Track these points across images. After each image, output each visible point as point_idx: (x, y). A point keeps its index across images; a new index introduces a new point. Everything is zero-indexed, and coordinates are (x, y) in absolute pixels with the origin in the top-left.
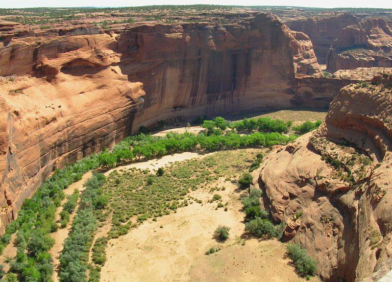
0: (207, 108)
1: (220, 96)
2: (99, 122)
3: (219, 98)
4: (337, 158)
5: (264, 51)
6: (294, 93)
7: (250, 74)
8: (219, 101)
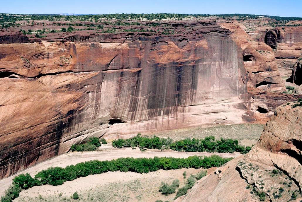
0: (148, 124)
1: (162, 112)
2: (19, 138)
3: (162, 114)
4: (262, 188)
5: (213, 63)
6: (246, 108)
7: (196, 89)
8: (161, 117)
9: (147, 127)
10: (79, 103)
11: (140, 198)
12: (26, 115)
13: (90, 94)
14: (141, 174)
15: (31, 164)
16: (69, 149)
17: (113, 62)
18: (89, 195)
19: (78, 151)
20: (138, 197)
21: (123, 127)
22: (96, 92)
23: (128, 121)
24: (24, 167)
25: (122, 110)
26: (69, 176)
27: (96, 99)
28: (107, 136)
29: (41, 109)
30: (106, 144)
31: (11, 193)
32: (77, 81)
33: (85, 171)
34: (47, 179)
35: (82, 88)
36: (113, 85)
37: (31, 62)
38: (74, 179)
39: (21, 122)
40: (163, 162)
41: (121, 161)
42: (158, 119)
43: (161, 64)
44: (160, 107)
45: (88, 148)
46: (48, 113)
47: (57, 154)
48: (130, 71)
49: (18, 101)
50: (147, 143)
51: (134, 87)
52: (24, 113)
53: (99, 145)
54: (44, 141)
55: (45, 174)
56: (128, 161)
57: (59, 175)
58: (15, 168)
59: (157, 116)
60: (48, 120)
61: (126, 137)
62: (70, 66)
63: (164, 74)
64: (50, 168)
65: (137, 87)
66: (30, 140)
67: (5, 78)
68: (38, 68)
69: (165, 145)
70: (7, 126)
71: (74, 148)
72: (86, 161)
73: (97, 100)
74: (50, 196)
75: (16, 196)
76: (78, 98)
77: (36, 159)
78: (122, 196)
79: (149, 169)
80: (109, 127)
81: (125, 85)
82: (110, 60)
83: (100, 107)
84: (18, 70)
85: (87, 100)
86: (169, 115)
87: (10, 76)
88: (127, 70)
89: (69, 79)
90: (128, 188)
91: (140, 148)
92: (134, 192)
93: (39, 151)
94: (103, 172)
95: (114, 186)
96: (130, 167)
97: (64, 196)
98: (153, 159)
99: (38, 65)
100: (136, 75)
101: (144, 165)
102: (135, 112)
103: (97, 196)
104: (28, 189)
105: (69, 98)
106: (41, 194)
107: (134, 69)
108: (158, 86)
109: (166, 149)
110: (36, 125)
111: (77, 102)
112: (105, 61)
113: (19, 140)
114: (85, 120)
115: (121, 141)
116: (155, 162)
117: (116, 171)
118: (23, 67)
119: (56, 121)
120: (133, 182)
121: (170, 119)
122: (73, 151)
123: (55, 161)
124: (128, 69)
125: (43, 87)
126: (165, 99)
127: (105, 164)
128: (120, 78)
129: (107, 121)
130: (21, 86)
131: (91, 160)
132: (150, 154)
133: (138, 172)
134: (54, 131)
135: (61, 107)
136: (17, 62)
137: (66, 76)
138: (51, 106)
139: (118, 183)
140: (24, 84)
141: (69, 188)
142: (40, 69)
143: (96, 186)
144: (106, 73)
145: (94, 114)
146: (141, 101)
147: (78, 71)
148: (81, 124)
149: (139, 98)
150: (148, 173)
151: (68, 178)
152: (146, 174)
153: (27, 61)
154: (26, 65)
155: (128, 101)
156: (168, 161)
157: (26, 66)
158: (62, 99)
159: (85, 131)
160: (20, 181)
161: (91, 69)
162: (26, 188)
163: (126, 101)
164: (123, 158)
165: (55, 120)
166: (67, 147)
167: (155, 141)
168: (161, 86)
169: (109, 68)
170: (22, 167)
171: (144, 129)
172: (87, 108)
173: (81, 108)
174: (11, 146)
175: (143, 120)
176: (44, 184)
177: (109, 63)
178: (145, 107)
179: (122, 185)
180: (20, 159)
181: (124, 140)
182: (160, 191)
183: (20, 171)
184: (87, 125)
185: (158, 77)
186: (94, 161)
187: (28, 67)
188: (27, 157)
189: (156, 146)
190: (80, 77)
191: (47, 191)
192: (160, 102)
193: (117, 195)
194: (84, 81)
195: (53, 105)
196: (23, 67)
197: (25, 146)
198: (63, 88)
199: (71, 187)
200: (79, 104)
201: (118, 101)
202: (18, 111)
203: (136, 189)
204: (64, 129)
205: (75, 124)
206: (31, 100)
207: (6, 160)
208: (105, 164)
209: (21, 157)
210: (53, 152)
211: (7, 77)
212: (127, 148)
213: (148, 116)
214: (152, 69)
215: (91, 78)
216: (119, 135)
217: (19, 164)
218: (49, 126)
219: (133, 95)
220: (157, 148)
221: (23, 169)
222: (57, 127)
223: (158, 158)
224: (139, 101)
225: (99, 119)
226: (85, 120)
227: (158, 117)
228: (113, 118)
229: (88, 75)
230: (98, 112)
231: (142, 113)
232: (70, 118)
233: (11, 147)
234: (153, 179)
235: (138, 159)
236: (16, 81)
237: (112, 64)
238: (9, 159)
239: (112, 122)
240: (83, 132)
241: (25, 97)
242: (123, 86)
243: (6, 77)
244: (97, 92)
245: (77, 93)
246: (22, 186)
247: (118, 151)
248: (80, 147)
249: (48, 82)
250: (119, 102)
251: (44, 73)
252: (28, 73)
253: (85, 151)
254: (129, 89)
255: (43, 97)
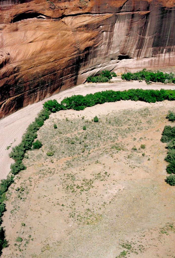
0: (152, 60)
1: (165, 50)
2: (46, 70)
8: (163, 55)
9: (151, 63)
10: (95, 41)
11: (150, 123)
12: (51, 50)
13: (104, 33)
14: (149, 103)
15: (55, 92)
16: (86, 80)
17: (125, 5)
18: (107, 119)
19: (93, 82)
20: (149, 122)
21: (130, 63)
22: (109, 32)
23: (134, 58)
24: (50, 94)
25: (130, 48)
26: (89, 103)
27: (109, 38)
28: (116, 70)
29: (63, 46)
30: (116, 77)
31: (43, 115)
32: (94, 22)
33: (102, 99)
34: (71, 105)
35: (98, 28)
36: (124, 26)
37: (55, 5)
38: (93, 106)
39: (46, 56)
40: (168, 94)
41: (132, 92)
42: (161, 56)
43: (167, 7)
44: (164, 46)
45: (101, 80)
46: (69, 49)
47: (75, 84)
48: (139, 13)
49: (44, 38)
50: (153, 77)
51: (142, 27)
52: (50, 49)
53: (110, 77)
54: (66, 73)
55: (69, 100)
56: (138, 92)
57: (81, 101)
58: (43, 95)
59: (159, 54)
60: (69, 55)
61: (133, 71)
62: (88, 8)
63: (169, 17)
64: (73, 95)
65: (144, 28)
66: (54, 72)
67: (33, 19)
68: (62, 10)
69: (168, 79)
70: (36, 59)
71: (89, 80)
72: (102, 91)
73: (110, 39)
74: (75, 119)
75: (47, 118)
76: (94, 36)
77: (59, 88)
78: (134, 121)
79: (156, 99)
80: (118, 62)
81: (135, 26)
82: (122, 3)
83: (112, 44)
84: (45, 11)
85: (101, 38)
86: (170, 53)
87: (38, 17)
88: (137, 12)
89: (87, 20)
90: (139, 114)
91: (146, 81)
92: (145, 118)
93: (62, 81)
94: (117, 100)
95: (127, 112)
96: (140, 97)
97: (86, 119)
98: (159, 90)
99: (61, 7)
100: (145, 17)
101: (152, 96)
102: (141, 50)
103: (114, 120)
104: (55, 112)
105: (87, 37)
106: (67, 117)
107: (144, 11)
108: (163, 28)
109: (168, 82)
110: (59, 59)
111: (93, 40)
112: (119, 4)
113: (46, 72)
114: (99, 56)
115: (130, 75)
116: (161, 93)
117: (127, 100)
118: (49, 9)
119: (75, 56)
120: (143, 109)
121: (171, 56)
122: (89, 82)
123: (74, 90)
124: (138, 12)
125: (65, 27)
126: (168, 39)
127: (119, 94)
128: (130, 20)
129: (117, 57)
130: (47, 25)
131: (106, 90)
132: (156, 87)
133: (146, 102)
134: (74, 64)
135: (80, 44)
136: (44, 5)
137: (84, 17)
138: (72, 43)
139: (158, 108)
140: (50, 24)
141: (90, 113)
142: (63, 11)
143: (112, 112)
144: (119, 15)
145: (107, 50)
146: (148, 40)
147: (94, 13)
148: (95, 59)
149: (146, 37)
150: (155, 102)
151: (88, 104)
152: (153, 103)
153: (52, 4)
154: (51, 7)
155: (136, 40)
156: (173, 93)
157: (51, 8)
158: (81, 38)
159: (99, 65)
160: (49, 105)
161: (106, 11)
162: (54, 112)
163: (135, 40)
164: (134, 89)
165: (75, 55)
166: (84, 78)
167: (159, 75)
168: (166, 28)
169: (122, 10)
170: (48, 95)
171: (148, 65)
172: (101, 46)
173: (96, 46)
174: (39, 76)
175: (147, 57)
176: (69, 109)
177: (121, 6)
178: (151, 45)
179: (134, 111)
180: (47, 88)
181: (132, 73)
182: (167, 118)
183: (47, 98)
184: (100, 60)
185: (164, 19)
186: (109, 91)
187: (53, 9)
188: (52, 86)
189: (160, 80)
190: (97, 18)
191: (72, 114)
192: (164, 41)
193: (131, 120)
194: (100, 21)
195: (73, 42)
196: (49, 9)
197: (51, 77)
198: (81, 27)
199: (91, 112)
200: (95, 42)
201: (128, 39)
202: (44, 47)
203: (146, 116)
204: (82, 63)
205: (91, 58)
206: (56, 37)
207: (36, 88)
208: (119, 94)
209: (48, 86)
210: (72, 82)
211: (36, 18)
212: (134, 81)
213: (152, 53)
214: (159, 12)
215: (106, 19)
216: (127, 69)
217: (46, 92)
218: (69, 60)
219: (141, 35)
220: (160, 82)
221: (50, 95)
222: (76, 61)
223: (164, 90)
224: (146, 40)
225: (110, 55)
226: (99, 56)
227: (160, 54)
228: (121, 54)
229: (104, 17)
230: (110, 48)
231: (147, 50)
232: (87, 53)
233: (40, 77)
234: (160, 108)
235: (146, 90)
236: (43, 21)
237: (125, 7)
238: (39, 87)
239: (121, 58)
240: (96, 66)
241: (50, 35)
242: (133, 26)
243: (34, 18)
244: (110, 32)
245: (93, 32)
246: (50, 109)
247: (127, 83)
248: (95, 78)
249: (70, 22)
250: (128, 41)
251: (66, 14)
252: (53, 14)
253: (99, 82)
254: (138, 30)
255: (65, 35)
